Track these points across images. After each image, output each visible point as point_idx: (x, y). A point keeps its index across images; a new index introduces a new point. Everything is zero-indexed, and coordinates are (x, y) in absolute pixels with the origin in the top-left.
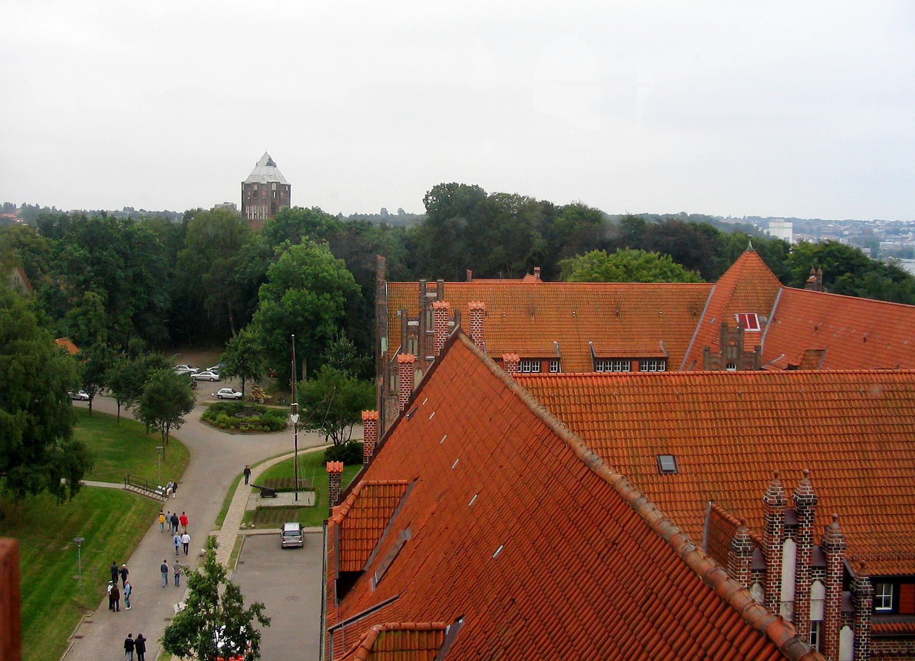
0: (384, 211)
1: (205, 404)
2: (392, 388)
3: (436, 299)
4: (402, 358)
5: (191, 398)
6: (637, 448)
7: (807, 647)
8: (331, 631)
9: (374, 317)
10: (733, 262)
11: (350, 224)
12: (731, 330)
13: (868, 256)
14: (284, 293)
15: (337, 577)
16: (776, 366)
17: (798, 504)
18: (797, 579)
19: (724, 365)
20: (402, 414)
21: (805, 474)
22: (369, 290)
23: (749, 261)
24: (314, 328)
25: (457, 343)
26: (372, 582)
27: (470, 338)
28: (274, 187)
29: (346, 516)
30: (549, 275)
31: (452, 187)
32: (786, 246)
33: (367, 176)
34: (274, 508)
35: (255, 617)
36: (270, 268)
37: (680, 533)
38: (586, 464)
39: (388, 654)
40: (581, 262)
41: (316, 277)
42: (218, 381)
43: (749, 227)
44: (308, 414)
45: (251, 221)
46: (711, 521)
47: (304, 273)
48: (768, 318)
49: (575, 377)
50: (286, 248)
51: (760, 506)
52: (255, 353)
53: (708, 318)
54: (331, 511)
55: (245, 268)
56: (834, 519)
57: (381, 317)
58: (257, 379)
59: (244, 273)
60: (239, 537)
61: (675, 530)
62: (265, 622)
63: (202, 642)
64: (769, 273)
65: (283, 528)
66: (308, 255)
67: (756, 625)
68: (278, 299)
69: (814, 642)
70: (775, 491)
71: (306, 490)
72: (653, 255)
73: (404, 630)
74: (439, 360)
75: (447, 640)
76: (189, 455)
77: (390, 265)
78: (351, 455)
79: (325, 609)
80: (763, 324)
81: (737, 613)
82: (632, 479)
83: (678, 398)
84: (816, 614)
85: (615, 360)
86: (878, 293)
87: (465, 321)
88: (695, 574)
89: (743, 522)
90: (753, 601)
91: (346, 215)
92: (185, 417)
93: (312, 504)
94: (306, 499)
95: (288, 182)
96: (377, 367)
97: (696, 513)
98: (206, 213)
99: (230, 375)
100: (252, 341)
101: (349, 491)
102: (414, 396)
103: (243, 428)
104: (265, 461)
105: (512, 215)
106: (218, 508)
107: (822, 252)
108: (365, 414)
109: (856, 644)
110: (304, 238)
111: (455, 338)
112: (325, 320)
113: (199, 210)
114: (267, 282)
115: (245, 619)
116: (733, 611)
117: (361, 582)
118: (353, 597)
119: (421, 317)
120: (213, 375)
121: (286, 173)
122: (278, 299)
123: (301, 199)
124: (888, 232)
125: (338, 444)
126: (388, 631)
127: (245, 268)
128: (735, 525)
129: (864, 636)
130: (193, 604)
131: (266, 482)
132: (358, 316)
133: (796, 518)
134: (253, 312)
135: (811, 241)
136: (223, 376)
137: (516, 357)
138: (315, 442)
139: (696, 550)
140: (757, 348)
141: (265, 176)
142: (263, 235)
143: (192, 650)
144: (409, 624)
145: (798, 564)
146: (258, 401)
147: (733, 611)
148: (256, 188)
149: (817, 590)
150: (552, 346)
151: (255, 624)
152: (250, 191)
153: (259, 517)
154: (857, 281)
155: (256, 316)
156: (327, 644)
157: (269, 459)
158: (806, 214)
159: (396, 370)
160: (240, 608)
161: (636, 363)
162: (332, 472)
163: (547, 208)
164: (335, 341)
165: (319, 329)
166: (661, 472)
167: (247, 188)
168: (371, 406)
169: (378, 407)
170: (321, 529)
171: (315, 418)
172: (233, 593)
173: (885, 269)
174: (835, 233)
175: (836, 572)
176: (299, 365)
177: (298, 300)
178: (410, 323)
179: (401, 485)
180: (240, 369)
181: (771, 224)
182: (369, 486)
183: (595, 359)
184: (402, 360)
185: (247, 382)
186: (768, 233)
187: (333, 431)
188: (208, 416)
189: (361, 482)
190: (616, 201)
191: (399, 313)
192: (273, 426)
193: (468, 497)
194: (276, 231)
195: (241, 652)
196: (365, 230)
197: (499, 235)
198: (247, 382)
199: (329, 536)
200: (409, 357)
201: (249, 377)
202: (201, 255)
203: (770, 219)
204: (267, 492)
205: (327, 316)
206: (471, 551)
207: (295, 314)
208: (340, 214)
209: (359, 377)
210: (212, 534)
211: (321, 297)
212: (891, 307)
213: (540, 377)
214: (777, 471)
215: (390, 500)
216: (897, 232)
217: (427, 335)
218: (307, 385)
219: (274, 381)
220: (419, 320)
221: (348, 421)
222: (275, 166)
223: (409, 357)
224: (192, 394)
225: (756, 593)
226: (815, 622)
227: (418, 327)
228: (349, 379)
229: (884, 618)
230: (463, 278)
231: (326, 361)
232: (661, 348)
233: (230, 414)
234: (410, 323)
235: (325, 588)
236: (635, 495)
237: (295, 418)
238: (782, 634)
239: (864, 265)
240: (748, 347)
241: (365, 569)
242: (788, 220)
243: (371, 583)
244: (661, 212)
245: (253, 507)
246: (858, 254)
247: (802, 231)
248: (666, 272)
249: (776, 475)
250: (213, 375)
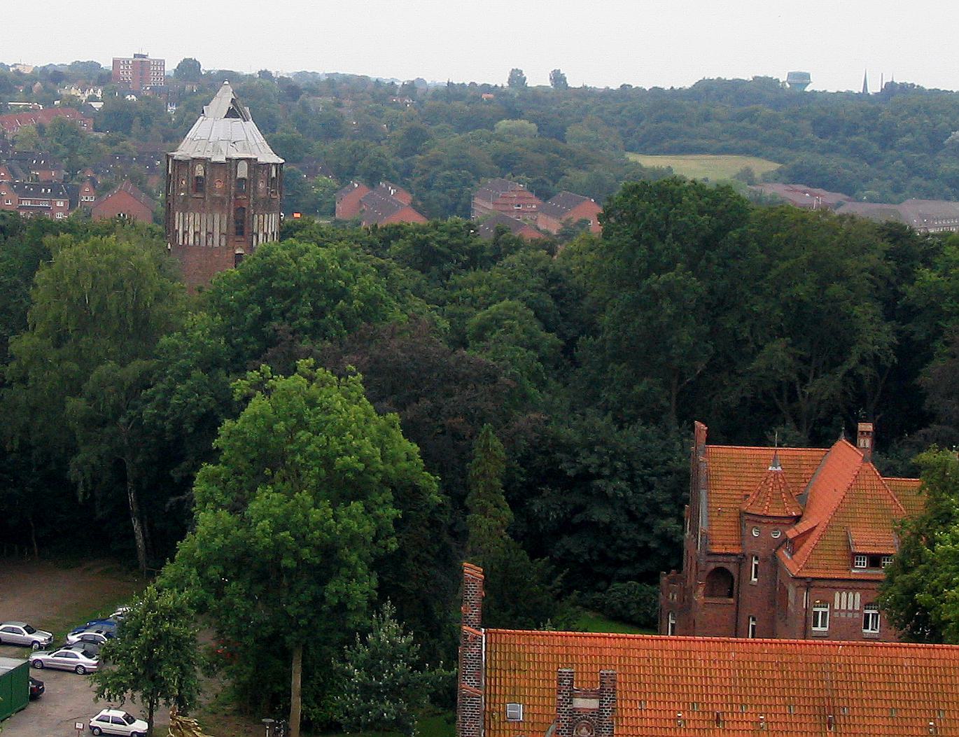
0: (517, 78)
24: (322, 582)
28: (243, 171)
45: (185, 247)
50: (259, 386)
55: (171, 391)
59: (164, 405)
66: (312, 403)
110: (302, 364)
120: (83, 660)
127: (171, 391)
148: (199, 171)
155: (183, 546)
165: (332, 587)
177: (287, 515)
197: (778, 312)
205: (354, 558)
211: (342, 512)
250: (83, 660)
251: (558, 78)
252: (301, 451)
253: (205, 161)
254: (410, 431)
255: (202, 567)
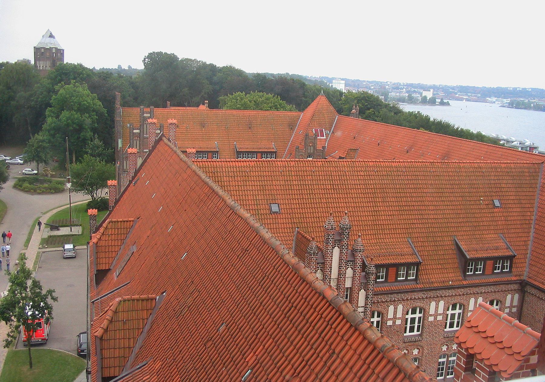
0: (119, 66)
1: (16, 178)
2: (125, 168)
3: (149, 118)
4: (130, 151)
5: (7, 174)
6: (259, 200)
7: (343, 300)
8: (93, 302)
9: (114, 127)
10: (312, 101)
11: (100, 73)
12: (310, 138)
13: (383, 100)
14: (61, 113)
15: (96, 273)
16: (333, 157)
17: (342, 229)
18: (340, 267)
19: (306, 156)
20: (131, 182)
21: (346, 213)
22: (111, 111)
23: (321, 101)
25: (161, 143)
26: (115, 275)
27: (169, 140)
28: (54, 51)
29: (100, 239)
30: (214, 105)
31: (160, 54)
32: (341, 93)
33: (108, 46)
34: (58, 236)
35: (49, 297)
36: (53, 98)
37: (281, 244)
38: (231, 208)
39: (125, 313)
40: (229, 99)
41: (80, 104)
42: (22, 164)
43: (322, 82)
44: (77, 183)
45: (40, 70)
46: (297, 238)
47: (73, 102)
48: (330, 132)
49: (226, 161)
51: (322, 230)
52: (44, 148)
53: (298, 132)
54: (91, 237)
56: (359, 236)
57: (118, 128)
58: (46, 162)
60: (38, 253)
61: (278, 243)
62: (55, 299)
63: (19, 312)
64: (332, 108)
65: (64, 247)
66: (75, 91)
67: (318, 290)
68: (57, 117)
69: (347, 298)
70: (330, 222)
71: (77, 225)
72: (270, 95)
73: (133, 300)
74: (151, 152)
75: (157, 305)
76: (6, 208)
77: (123, 97)
78: (102, 205)
79: (89, 291)
80: (327, 135)
81: (309, 284)
82: (256, 217)
83: (281, 173)
84: (348, 284)
85: (248, 152)
86: (385, 120)
87: (165, 131)
88: (288, 266)
89: (313, 239)
90: (317, 278)
91: (98, 68)
92: (3, 186)
93: (80, 233)
94: (77, 230)
95: (62, 48)
96: (116, 155)
97: (290, 234)
98: (12, 64)
99: (30, 161)
100: (43, 141)
101: (101, 225)
102: (137, 172)
103: (39, 191)
104: (52, 210)
105: (193, 71)
106: (25, 237)
107: (359, 97)
108: (110, 182)
109: (367, 298)
110: (72, 81)
111: (160, 139)
112: (85, 129)
113: (7, 63)
114: (51, 107)
115: (44, 298)
116: (307, 284)
117: (109, 275)
118: (105, 283)
119: (141, 128)
120: (20, 161)
121: (61, 42)
122: (57, 117)
123: (70, 58)
124: (393, 88)
125: (94, 200)
126: (125, 301)
128: (309, 241)
129: (370, 294)
130: (12, 292)
131: (53, 222)
132: (106, 129)
133: (341, 236)
134: (43, 124)
135: (354, 91)
136: (26, 162)
137: (194, 151)
138: (82, 198)
139: (289, 253)
140: (324, 147)
141: (49, 43)
142: (48, 79)
143: (13, 318)
144: (136, 297)
145: (340, 259)
146: (47, 175)
147: (307, 284)
148: (43, 50)
149: (349, 272)
150: (214, 145)
151: (49, 301)
152: (39, 52)
153: (49, 241)
154: (377, 113)
155: (45, 126)
156: (91, 309)
157: (54, 209)
158: (352, 77)
159: (127, 158)
160: (40, 292)
161: (259, 155)
162: (91, 215)
163: (212, 67)
164: (92, 141)
166: (272, 213)
167: (37, 50)
168: (114, 178)
169: (117, 178)
170: (85, 247)
171: (81, 185)
172: (36, 284)
173: (391, 108)
174: (366, 87)
175: (359, 263)
176: (71, 154)
178: (135, 131)
179: (130, 221)
180: (35, 157)
181: (334, 81)
182: (112, 222)
183: (237, 152)
184: (129, 150)
185: (40, 165)
186: (332, 86)
187: (91, 192)
188: (17, 185)
189: (108, 220)
190: (252, 65)
191: (128, 125)
192: (57, 190)
193: (167, 227)
194: (56, 77)
195: (42, 316)
196: (109, 78)
198: (40, 165)
199: (90, 251)
200: (134, 150)
201: (42, 162)
202: (10, 90)
203: (333, 79)
204: (54, 227)
206: (169, 257)
207: (68, 125)
208: (94, 68)
209: (106, 161)
210: (23, 252)
212: (392, 128)
213: (207, 162)
214: (331, 212)
215: (125, 228)
216: (397, 88)
217: (144, 138)
218: (76, 167)
219: (56, 164)
220: (140, 129)
221: (100, 186)
222: (54, 38)
223: (134, 150)
224: (7, 172)
225: (319, 275)
226: (347, 288)
227: (140, 134)
228: (100, 163)
229: (381, 285)
230: (165, 106)
231: (87, 153)
232: (273, 146)
233: (30, 183)
234: (135, 131)
235: (89, 279)
236: (257, 225)
237: (69, 185)
238: (330, 294)
239: (379, 105)
240: (319, 147)
241: (111, 268)
242: (342, 79)
243: (114, 276)
244: (275, 72)
245: (46, 236)
246: (377, 99)
247: (350, 85)
248: (276, 105)
249: (331, 214)
250: (20, 161)
251: (129, 67)
252: (73, 102)
253: (44, 48)
254: (99, 99)
255: (49, 131)
